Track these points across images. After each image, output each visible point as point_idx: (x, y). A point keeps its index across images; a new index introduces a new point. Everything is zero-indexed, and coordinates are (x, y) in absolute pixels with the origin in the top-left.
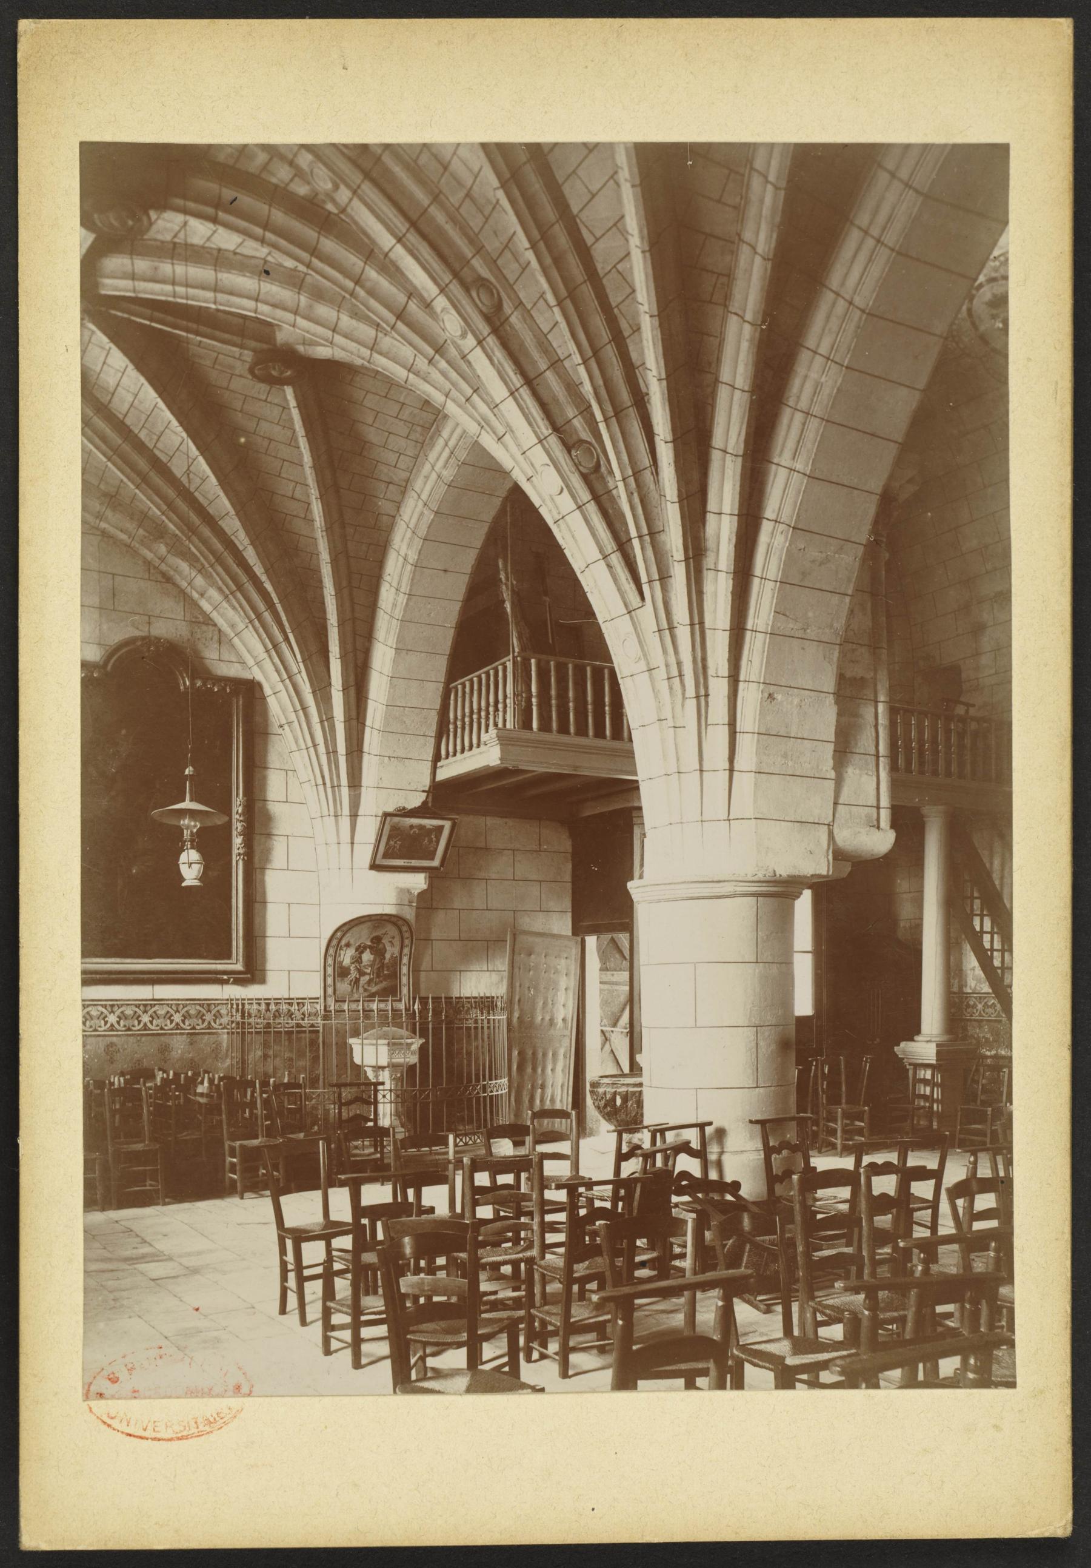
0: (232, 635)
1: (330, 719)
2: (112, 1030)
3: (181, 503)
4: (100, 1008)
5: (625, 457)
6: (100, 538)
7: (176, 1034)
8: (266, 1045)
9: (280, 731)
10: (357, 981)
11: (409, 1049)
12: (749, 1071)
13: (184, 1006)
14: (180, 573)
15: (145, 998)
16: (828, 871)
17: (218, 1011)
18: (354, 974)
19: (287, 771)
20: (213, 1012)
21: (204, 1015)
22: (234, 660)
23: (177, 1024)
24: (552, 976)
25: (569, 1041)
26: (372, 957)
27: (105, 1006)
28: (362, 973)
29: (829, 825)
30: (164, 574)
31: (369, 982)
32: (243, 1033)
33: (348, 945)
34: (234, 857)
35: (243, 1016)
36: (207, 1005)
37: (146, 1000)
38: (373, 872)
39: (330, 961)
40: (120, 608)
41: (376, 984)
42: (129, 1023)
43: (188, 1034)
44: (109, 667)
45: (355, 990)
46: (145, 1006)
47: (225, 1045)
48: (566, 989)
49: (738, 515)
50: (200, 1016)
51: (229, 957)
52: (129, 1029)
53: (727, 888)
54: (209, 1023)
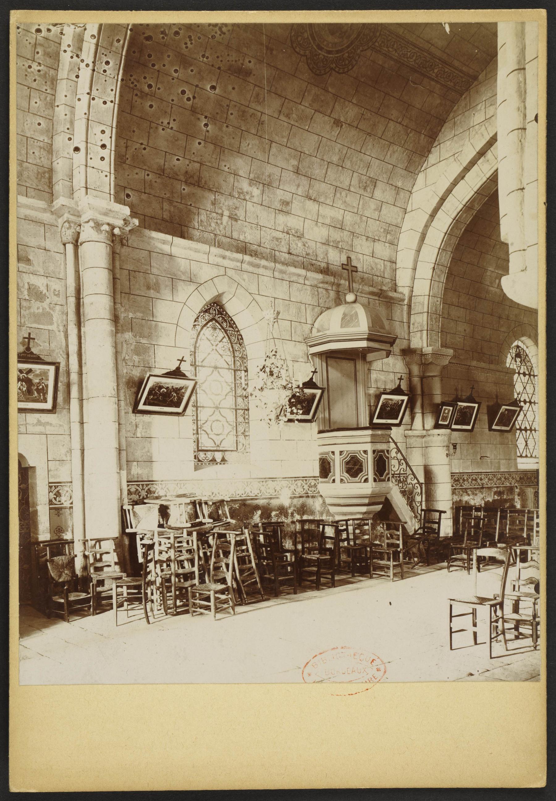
13: (147, 485)
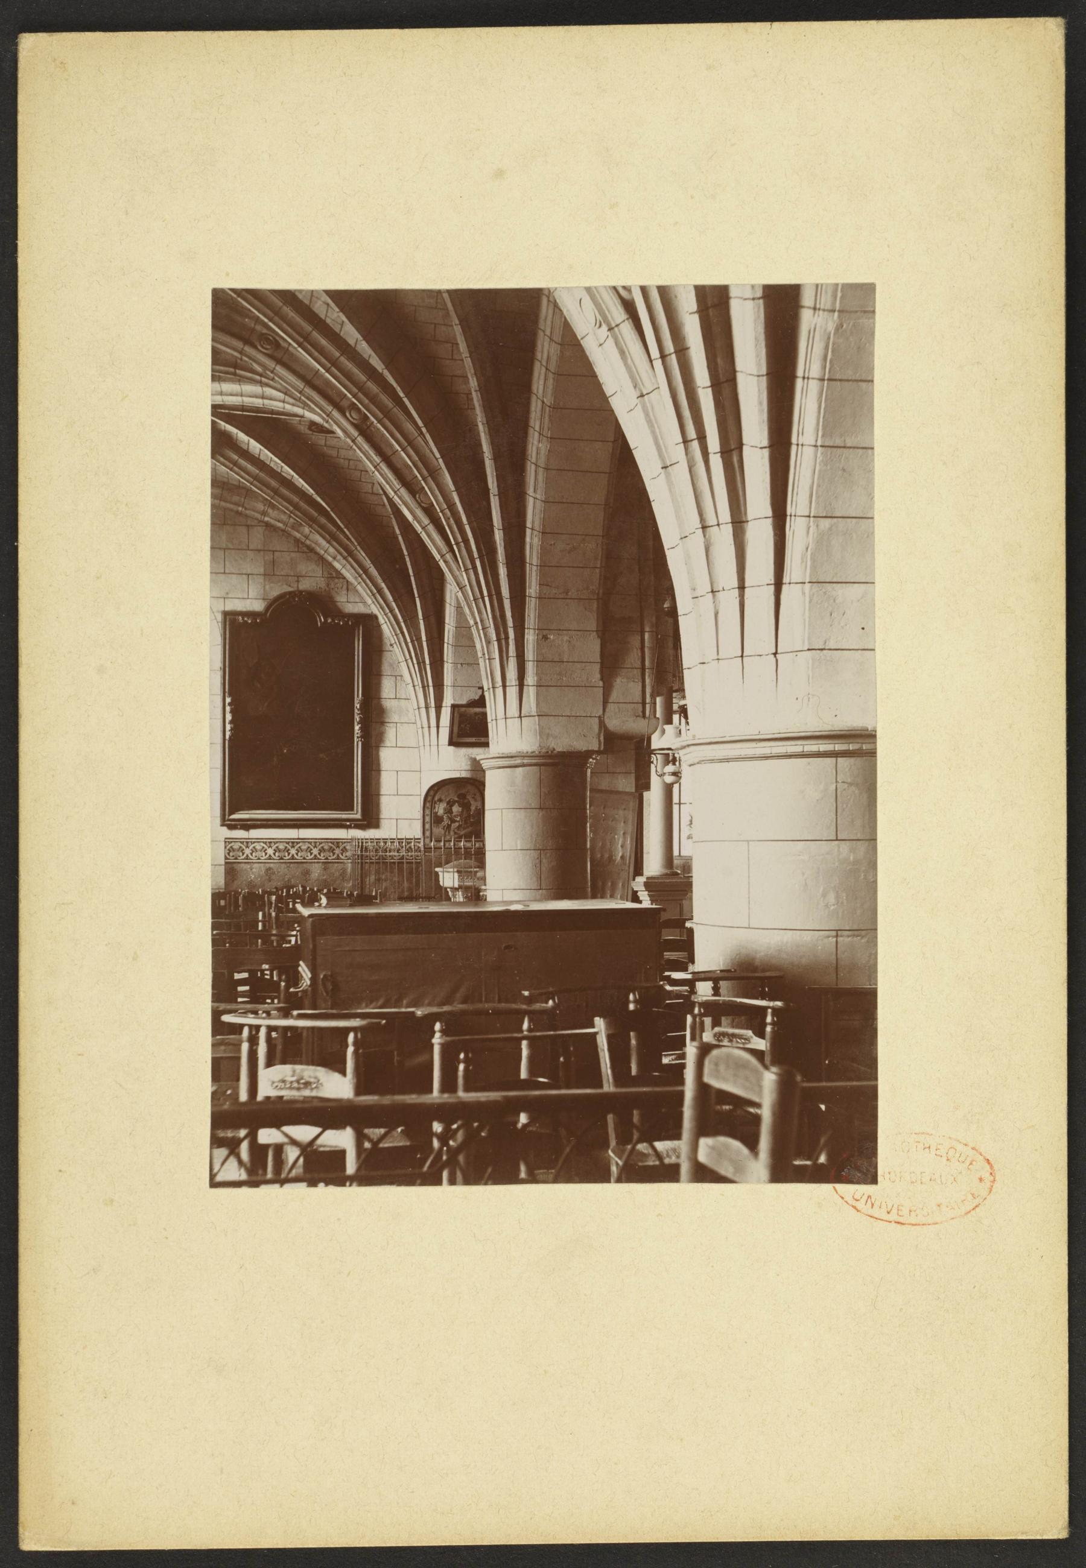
0: (356, 583)
1: (419, 639)
2: (270, 859)
3: (303, 504)
4: (262, 844)
5: (440, 498)
6: (264, 528)
7: (314, 862)
8: (378, 872)
9: (391, 649)
10: (449, 827)
11: (475, 875)
12: (535, 879)
13: (320, 843)
14: (319, 545)
15: (292, 837)
16: (599, 747)
17: (345, 847)
18: (446, 822)
19: (396, 676)
20: (341, 848)
21: (334, 850)
22: (358, 601)
23: (315, 856)
24: (610, 823)
25: (626, 874)
26: (460, 809)
27: (265, 843)
28: (453, 821)
29: (599, 717)
30: (308, 547)
31: (459, 828)
32: (362, 863)
33: (440, 800)
34: (355, 738)
35: (362, 851)
36: (337, 842)
37: (294, 839)
38: (452, 748)
39: (428, 812)
40: (278, 574)
41: (464, 829)
42: (282, 854)
43: (323, 862)
44: (268, 615)
45: (447, 833)
46: (293, 843)
47: (349, 870)
48: (624, 834)
49: (769, 447)
50: (332, 850)
51: (352, 809)
52: (282, 859)
53: (518, 761)
54: (338, 856)
